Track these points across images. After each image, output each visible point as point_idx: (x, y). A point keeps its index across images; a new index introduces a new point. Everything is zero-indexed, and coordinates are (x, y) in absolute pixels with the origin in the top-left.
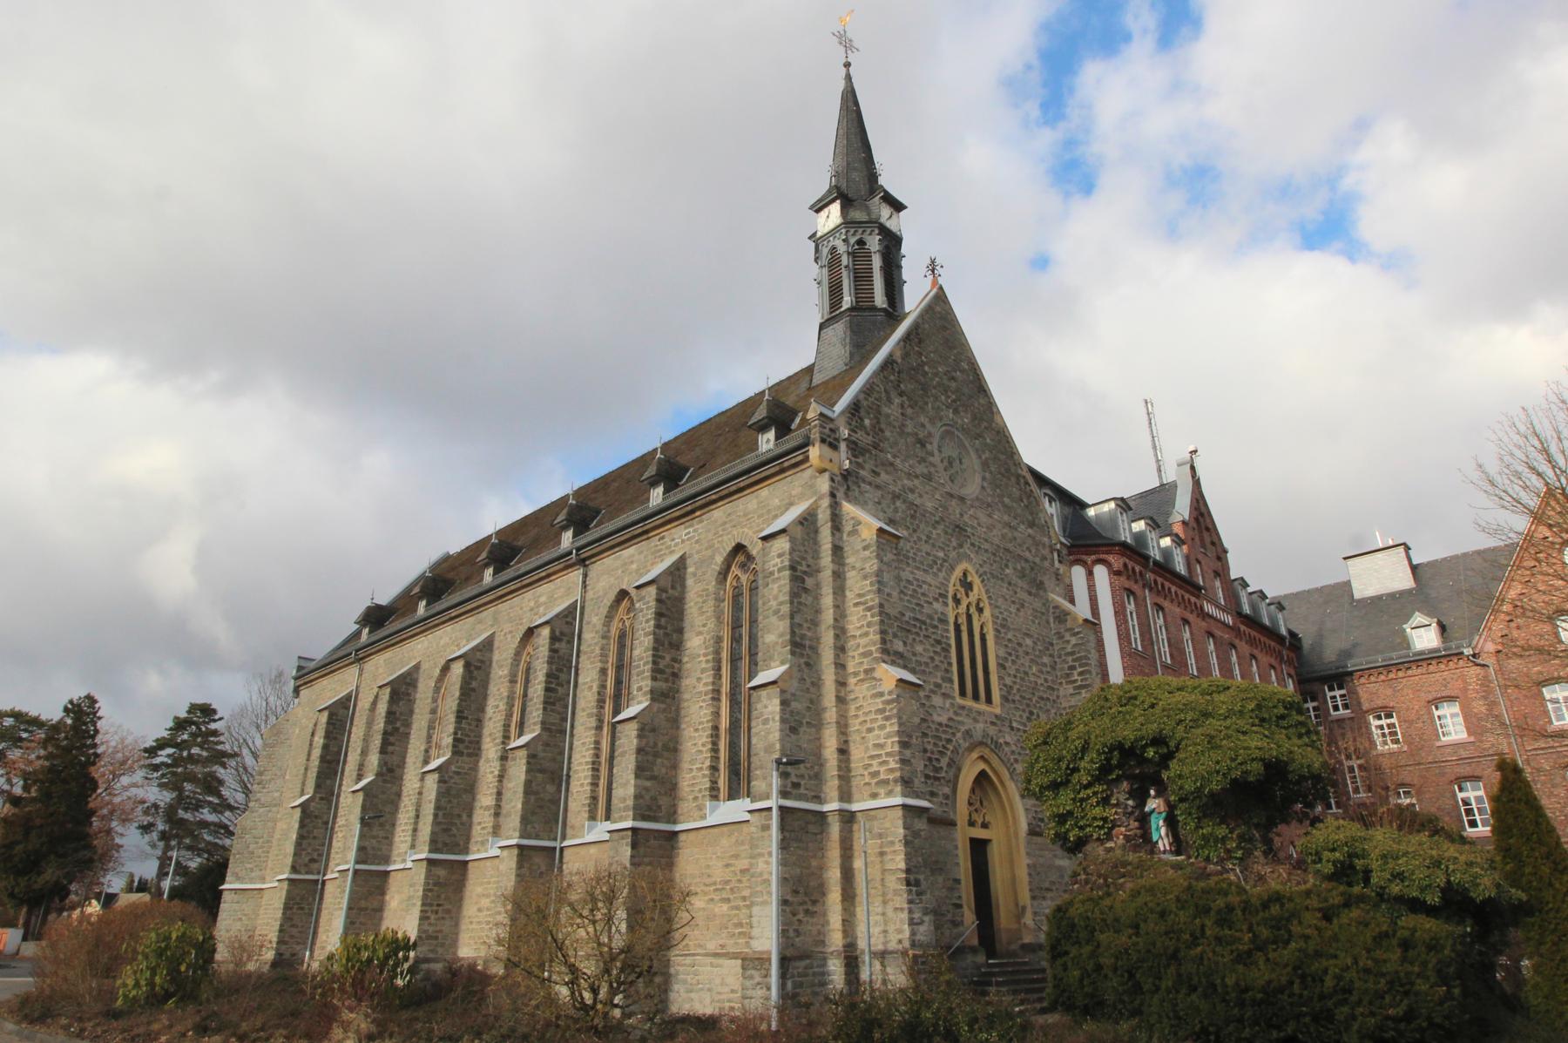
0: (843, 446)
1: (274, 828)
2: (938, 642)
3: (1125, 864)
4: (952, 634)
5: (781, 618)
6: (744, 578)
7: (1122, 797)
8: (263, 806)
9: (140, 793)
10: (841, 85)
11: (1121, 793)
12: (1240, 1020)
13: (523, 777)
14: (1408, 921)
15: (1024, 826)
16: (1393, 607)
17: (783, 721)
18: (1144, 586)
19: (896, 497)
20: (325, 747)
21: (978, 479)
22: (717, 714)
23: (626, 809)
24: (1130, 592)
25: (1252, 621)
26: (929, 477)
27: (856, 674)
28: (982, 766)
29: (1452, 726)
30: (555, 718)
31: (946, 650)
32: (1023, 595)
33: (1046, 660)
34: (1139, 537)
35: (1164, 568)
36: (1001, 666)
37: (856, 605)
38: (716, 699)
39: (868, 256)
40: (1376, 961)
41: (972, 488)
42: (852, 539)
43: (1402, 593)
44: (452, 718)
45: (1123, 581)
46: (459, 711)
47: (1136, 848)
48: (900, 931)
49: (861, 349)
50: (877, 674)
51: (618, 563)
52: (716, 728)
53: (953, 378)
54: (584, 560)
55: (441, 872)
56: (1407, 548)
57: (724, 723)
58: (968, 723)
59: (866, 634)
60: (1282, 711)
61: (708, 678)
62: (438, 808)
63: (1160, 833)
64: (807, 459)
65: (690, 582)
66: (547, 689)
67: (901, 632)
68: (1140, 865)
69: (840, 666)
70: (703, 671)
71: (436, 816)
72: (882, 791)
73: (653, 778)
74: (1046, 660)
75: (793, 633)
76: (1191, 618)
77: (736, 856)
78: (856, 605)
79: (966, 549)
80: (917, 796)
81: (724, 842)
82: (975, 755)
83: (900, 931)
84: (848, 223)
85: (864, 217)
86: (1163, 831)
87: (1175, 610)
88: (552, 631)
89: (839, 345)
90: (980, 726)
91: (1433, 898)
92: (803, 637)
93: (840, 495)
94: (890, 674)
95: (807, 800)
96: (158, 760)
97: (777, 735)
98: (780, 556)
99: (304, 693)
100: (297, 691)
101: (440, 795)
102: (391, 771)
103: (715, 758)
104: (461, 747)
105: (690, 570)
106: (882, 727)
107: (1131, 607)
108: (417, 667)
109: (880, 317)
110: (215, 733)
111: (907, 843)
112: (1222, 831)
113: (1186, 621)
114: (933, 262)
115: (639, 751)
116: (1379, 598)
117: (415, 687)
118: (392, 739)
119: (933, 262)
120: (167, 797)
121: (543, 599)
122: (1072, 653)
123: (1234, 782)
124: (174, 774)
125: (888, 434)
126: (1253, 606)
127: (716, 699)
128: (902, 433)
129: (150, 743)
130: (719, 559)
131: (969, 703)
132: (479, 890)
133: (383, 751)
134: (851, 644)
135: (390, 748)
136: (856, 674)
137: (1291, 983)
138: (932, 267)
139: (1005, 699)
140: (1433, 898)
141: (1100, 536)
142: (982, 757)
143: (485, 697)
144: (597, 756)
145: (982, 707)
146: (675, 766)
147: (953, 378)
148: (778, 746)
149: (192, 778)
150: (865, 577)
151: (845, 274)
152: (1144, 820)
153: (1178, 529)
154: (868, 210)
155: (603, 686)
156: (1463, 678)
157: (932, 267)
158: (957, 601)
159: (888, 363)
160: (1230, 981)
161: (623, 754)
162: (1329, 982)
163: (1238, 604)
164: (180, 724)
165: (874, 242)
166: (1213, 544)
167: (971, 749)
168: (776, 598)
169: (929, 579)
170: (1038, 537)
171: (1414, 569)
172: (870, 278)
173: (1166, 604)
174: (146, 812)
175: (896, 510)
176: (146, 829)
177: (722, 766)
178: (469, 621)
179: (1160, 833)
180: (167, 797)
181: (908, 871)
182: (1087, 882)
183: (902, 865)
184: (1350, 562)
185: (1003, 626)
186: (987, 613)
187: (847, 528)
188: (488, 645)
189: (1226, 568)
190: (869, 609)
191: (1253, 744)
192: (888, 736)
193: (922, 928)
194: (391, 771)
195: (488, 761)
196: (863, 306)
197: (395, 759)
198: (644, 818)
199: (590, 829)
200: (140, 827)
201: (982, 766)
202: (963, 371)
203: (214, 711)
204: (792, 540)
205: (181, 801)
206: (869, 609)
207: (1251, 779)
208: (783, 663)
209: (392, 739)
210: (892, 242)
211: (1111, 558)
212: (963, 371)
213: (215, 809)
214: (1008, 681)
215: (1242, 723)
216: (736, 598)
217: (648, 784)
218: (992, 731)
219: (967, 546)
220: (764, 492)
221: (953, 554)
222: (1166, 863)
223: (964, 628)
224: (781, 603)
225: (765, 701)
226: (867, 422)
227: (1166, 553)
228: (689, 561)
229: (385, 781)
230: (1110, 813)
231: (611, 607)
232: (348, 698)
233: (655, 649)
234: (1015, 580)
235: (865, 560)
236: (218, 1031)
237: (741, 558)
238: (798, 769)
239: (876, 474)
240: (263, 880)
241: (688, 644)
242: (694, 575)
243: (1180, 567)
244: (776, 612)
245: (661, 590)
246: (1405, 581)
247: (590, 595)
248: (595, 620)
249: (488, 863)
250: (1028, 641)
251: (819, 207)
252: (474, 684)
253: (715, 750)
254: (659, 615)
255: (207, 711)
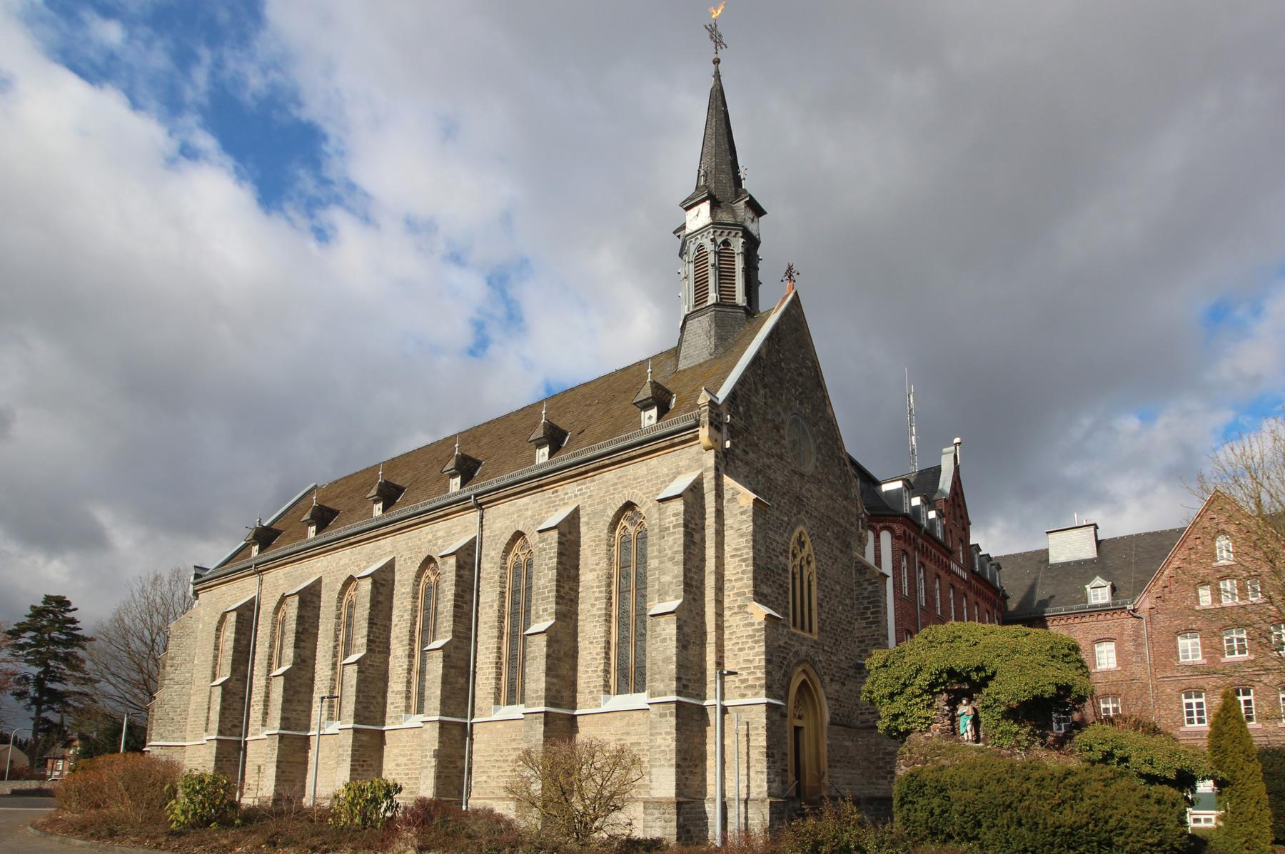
0: (725, 429)
1: (189, 700)
2: (781, 586)
3: (940, 748)
4: (790, 581)
5: (676, 564)
6: (632, 530)
7: (941, 704)
8: (177, 683)
9: (10, 667)
10: (711, 82)
11: (941, 701)
12: (1052, 844)
13: (440, 671)
14: (1156, 790)
15: (827, 718)
16: (1080, 571)
17: (678, 640)
18: (915, 548)
19: (759, 472)
20: (237, 641)
21: (813, 459)
22: (609, 632)
23: (538, 698)
24: (905, 552)
25: (979, 577)
26: (781, 457)
27: (730, 608)
28: (803, 677)
29: (1106, 658)
30: (461, 629)
31: (786, 592)
32: (837, 552)
33: (847, 601)
34: (916, 510)
35: (929, 535)
36: (820, 605)
37: (733, 556)
38: (608, 621)
39: (732, 256)
40: (1143, 811)
41: (809, 468)
42: (731, 505)
43: (1086, 561)
44: (365, 624)
45: (901, 544)
46: (370, 619)
47: (947, 738)
48: (759, 786)
49: (727, 340)
50: (748, 610)
51: (513, 509)
52: (608, 642)
53: (800, 374)
54: (481, 505)
55: (364, 738)
56: (1096, 527)
57: (614, 639)
58: (797, 647)
59: (741, 579)
60: (1067, 651)
61: (601, 604)
62: (358, 691)
63: (965, 726)
64: (697, 438)
65: (583, 529)
66: (456, 606)
67: (768, 581)
68: (951, 749)
69: (719, 602)
70: (596, 599)
71: (357, 697)
72: (749, 693)
73: (557, 676)
74: (847, 601)
75: (685, 575)
76: (942, 573)
77: (628, 734)
78: (733, 556)
79: (802, 516)
80: (774, 698)
81: (617, 723)
82: (800, 669)
83: (759, 786)
84: (716, 224)
85: (731, 221)
86: (969, 728)
87: (931, 566)
88: (458, 561)
89: (704, 337)
90: (804, 648)
91: (1171, 775)
92: (691, 578)
93: (721, 469)
94: (760, 612)
95: (693, 697)
96: (22, 641)
97: (674, 651)
98: (675, 515)
99: (202, 595)
100: (196, 594)
101: (360, 682)
102: (304, 661)
103: (608, 664)
104: (373, 646)
105: (582, 520)
106: (751, 648)
107: (904, 563)
108: (319, 581)
109: (741, 313)
110: (73, 621)
111: (768, 730)
112: (1015, 728)
113: (938, 576)
114: (790, 268)
115: (548, 656)
116: (1068, 564)
117: (319, 597)
118: (302, 637)
119: (790, 268)
120: (35, 670)
121: (440, 534)
122: (868, 598)
123: (1035, 697)
124: (39, 652)
125: (755, 419)
126: (982, 566)
127: (608, 621)
128: (765, 420)
129: (12, 627)
130: (611, 513)
131: (798, 632)
132: (396, 751)
133: (296, 646)
134: (727, 585)
135: (302, 644)
136: (730, 608)
137: (1088, 823)
138: (790, 274)
139: (821, 629)
140: (1171, 775)
141: (889, 509)
142: (804, 671)
143: (391, 608)
144: (500, 658)
145: (807, 635)
146: (574, 668)
147: (800, 374)
148: (674, 659)
149: (56, 656)
150: (742, 536)
151: (711, 271)
152: (953, 720)
153: (941, 506)
154: (733, 212)
155: (502, 606)
156: (1122, 626)
157: (790, 274)
158: (794, 556)
159: (757, 359)
160: (1050, 821)
161: (534, 658)
162: (1112, 823)
163: (973, 565)
164: (38, 613)
165: (738, 244)
166: (961, 517)
167: (798, 664)
168: (671, 548)
169: (777, 538)
170: (850, 507)
171: (1098, 543)
172: (732, 277)
173: (927, 563)
174: (18, 682)
175: (758, 483)
176: (20, 695)
177: (612, 670)
178: (368, 547)
179: (965, 726)
180: (35, 670)
181: (768, 747)
182: (911, 758)
183: (764, 744)
184: (1050, 536)
185: (823, 575)
186: (813, 565)
187: (727, 496)
188: (390, 567)
189: (968, 537)
190: (744, 560)
191: (1050, 674)
192: (757, 654)
193: (775, 785)
194: (304, 661)
195: (396, 657)
196: (724, 302)
197: (307, 653)
198: (553, 705)
199: (496, 711)
200: (14, 694)
201: (803, 677)
202: (807, 368)
203: (69, 603)
204: (686, 504)
205: (49, 674)
206: (744, 560)
207: (1046, 696)
208: (676, 598)
209: (302, 637)
210: (752, 243)
211: (895, 526)
212: (807, 368)
213: (78, 681)
214: (824, 616)
215: (1041, 658)
216: (625, 544)
217: (555, 681)
218: (812, 652)
219: (803, 513)
220: (654, 462)
221: (794, 519)
222: (971, 748)
223: (798, 576)
224: (676, 552)
225: (663, 625)
226: (741, 409)
227: (932, 522)
228: (581, 512)
229: (300, 669)
230: (931, 713)
231: (508, 544)
232: (252, 602)
233: (558, 581)
234: (833, 541)
235: (742, 522)
236: (286, 844)
237: (629, 513)
238: (690, 677)
239: (746, 453)
240: (184, 739)
241: (582, 578)
242: (588, 523)
243: (939, 535)
244: (672, 559)
245: (561, 534)
246: (1090, 552)
247: (486, 533)
248: (493, 553)
249: (403, 732)
250: (838, 588)
251: (688, 206)
252: (381, 598)
253: (607, 658)
254: (560, 554)
255: (62, 603)
